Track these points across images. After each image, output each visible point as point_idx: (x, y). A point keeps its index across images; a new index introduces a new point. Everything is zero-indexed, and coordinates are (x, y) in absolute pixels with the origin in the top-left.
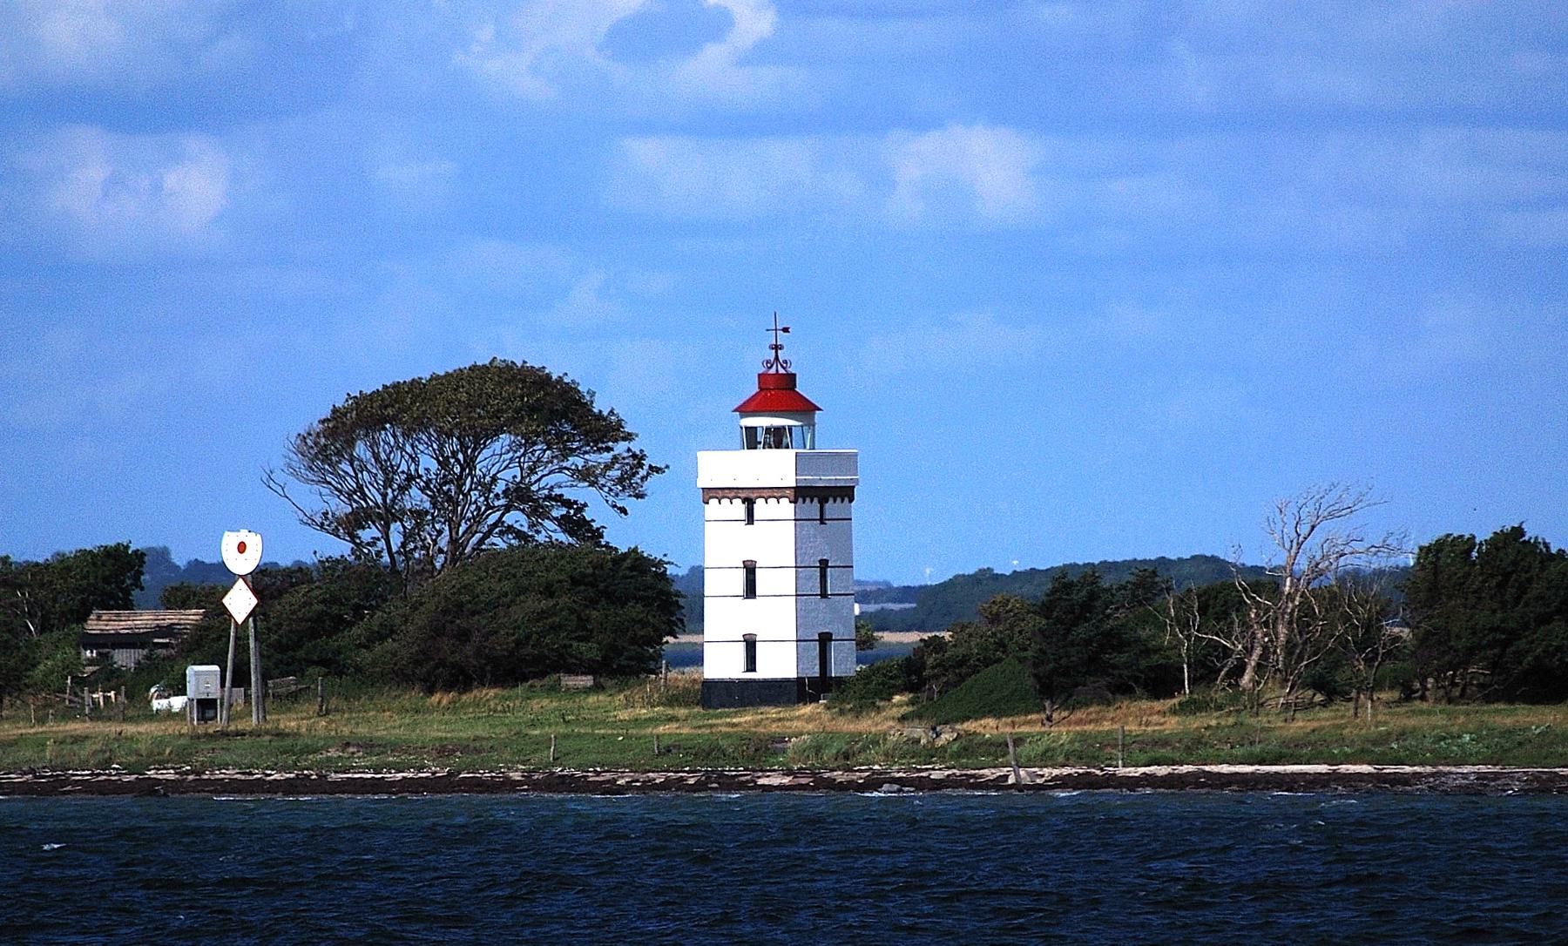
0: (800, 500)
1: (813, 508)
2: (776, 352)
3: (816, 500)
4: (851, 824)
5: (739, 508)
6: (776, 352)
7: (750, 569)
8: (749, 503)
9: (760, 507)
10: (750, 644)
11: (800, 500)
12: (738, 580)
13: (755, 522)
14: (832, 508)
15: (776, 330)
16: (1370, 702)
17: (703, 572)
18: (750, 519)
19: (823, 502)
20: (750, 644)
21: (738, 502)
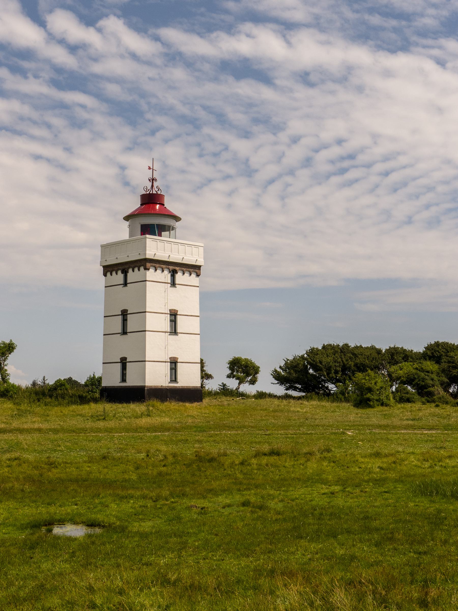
0: (109, 274)
1: (119, 277)
2: (153, 183)
3: (119, 272)
4: (385, 427)
5: (120, 276)
6: (153, 183)
7: (174, 315)
8: (173, 273)
9: (179, 277)
10: (174, 363)
11: (109, 274)
12: (166, 325)
13: (177, 286)
14: (132, 275)
15: (153, 169)
16: (57, 530)
17: (202, 309)
18: (173, 284)
19: (125, 272)
20: (174, 363)
21: (166, 272)
